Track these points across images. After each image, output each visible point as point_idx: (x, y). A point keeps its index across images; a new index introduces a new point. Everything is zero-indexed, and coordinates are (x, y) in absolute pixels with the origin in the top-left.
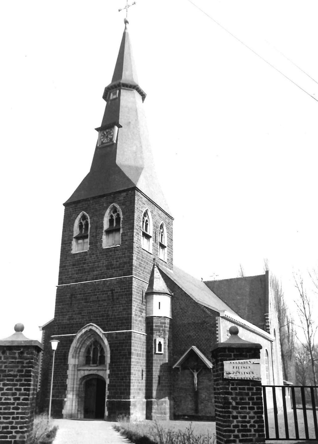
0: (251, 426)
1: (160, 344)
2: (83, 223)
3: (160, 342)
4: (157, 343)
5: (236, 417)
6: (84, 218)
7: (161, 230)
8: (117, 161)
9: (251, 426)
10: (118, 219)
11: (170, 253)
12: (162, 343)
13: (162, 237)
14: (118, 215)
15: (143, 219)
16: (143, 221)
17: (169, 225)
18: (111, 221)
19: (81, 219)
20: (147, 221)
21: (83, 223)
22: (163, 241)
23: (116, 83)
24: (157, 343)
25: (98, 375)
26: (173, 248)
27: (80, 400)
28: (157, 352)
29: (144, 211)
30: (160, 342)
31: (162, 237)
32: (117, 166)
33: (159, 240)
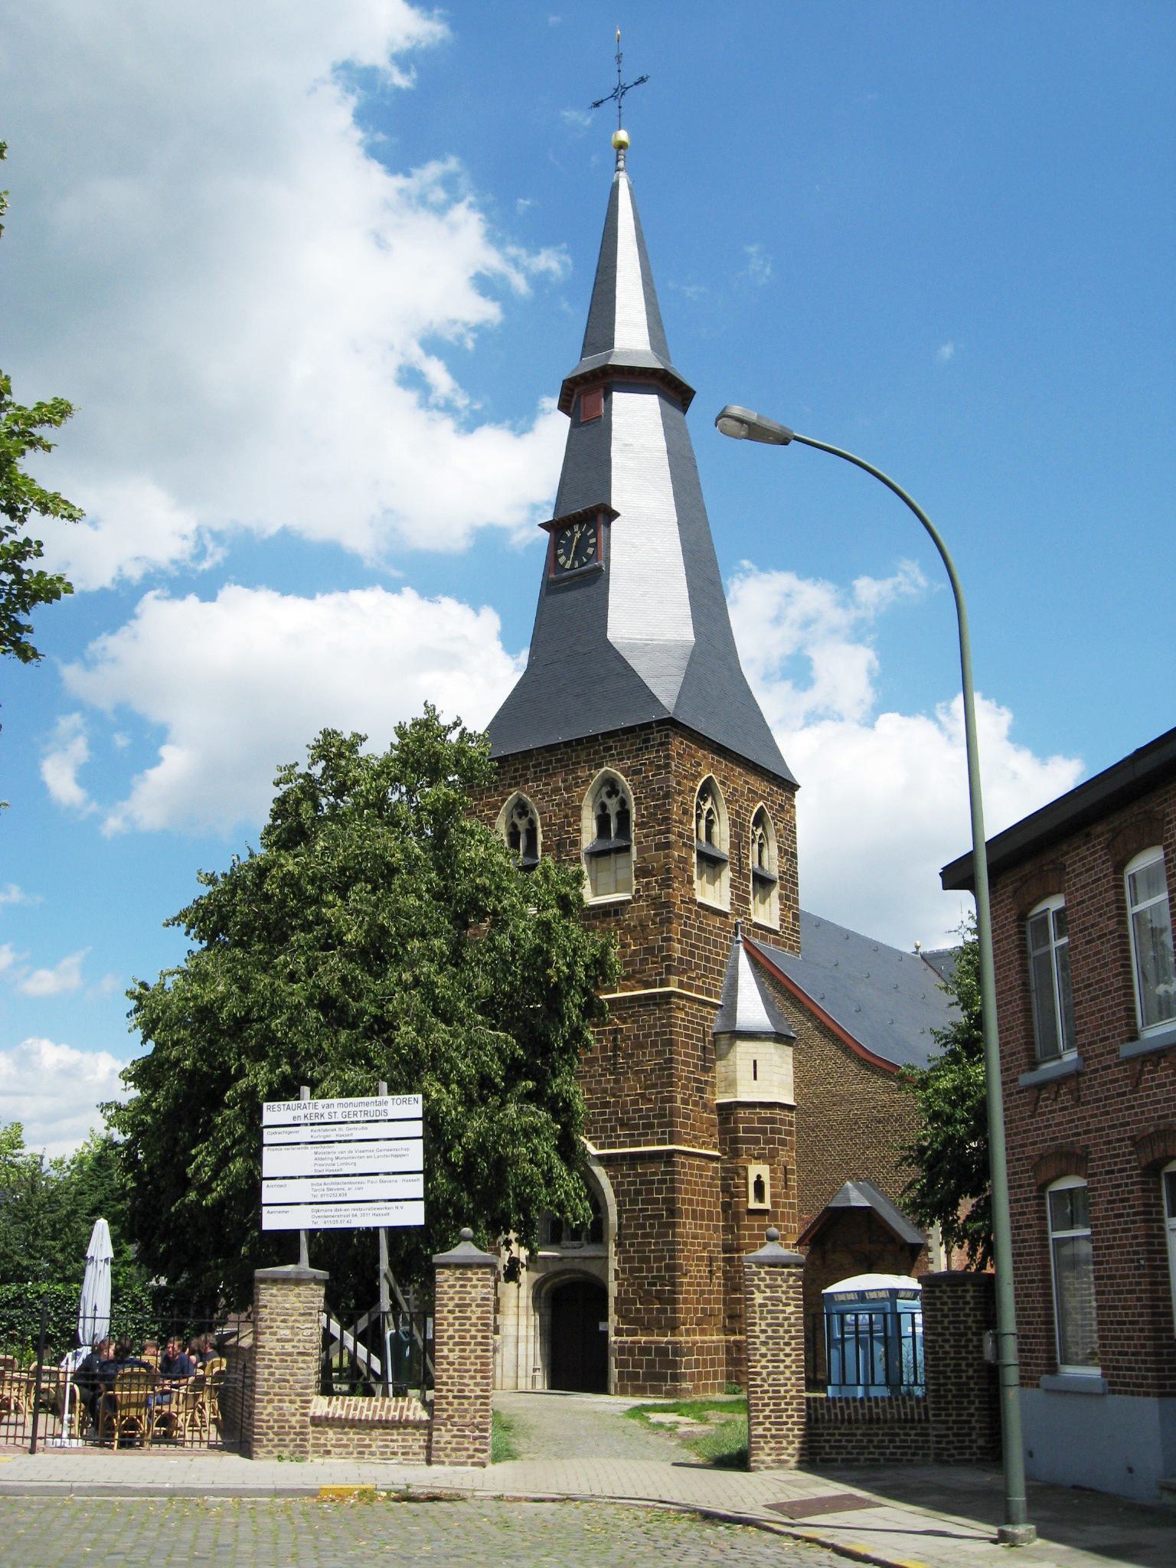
0: (453, 1325)
1: (759, 1185)
2: (522, 825)
3: (759, 1177)
4: (752, 1179)
5: (764, 1356)
6: (521, 808)
7: (760, 831)
8: (609, 636)
9: (453, 1325)
10: (624, 815)
11: (789, 900)
12: (766, 1179)
13: (760, 852)
14: (623, 803)
15: (699, 807)
16: (699, 816)
17: (786, 810)
18: (603, 822)
19: (515, 812)
20: (710, 812)
21: (522, 825)
22: (765, 864)
23: (593, 362)
24: (752, 1179)
25: (585, 1273)
26: (799, 882)
27: (131, 1250)
28: (753, 1205)
29: (494, 1503)
30: (759, 1177)
31: (760, 852)
32: (609, 646)
33: (752, 863)
